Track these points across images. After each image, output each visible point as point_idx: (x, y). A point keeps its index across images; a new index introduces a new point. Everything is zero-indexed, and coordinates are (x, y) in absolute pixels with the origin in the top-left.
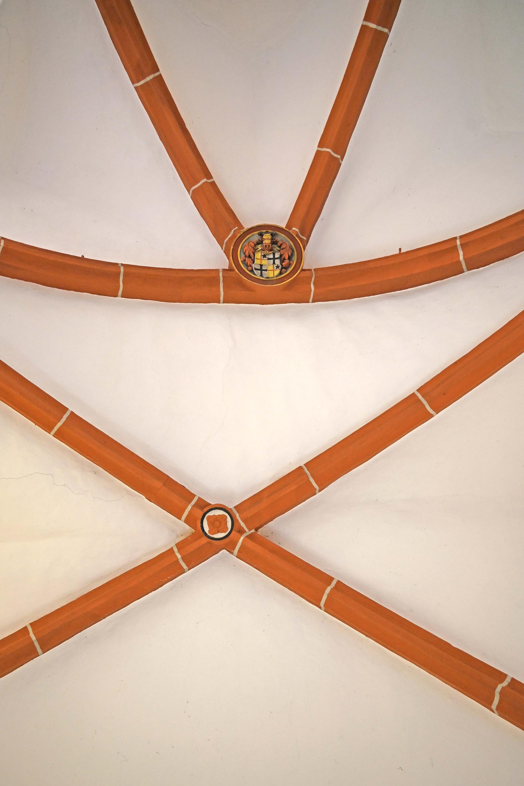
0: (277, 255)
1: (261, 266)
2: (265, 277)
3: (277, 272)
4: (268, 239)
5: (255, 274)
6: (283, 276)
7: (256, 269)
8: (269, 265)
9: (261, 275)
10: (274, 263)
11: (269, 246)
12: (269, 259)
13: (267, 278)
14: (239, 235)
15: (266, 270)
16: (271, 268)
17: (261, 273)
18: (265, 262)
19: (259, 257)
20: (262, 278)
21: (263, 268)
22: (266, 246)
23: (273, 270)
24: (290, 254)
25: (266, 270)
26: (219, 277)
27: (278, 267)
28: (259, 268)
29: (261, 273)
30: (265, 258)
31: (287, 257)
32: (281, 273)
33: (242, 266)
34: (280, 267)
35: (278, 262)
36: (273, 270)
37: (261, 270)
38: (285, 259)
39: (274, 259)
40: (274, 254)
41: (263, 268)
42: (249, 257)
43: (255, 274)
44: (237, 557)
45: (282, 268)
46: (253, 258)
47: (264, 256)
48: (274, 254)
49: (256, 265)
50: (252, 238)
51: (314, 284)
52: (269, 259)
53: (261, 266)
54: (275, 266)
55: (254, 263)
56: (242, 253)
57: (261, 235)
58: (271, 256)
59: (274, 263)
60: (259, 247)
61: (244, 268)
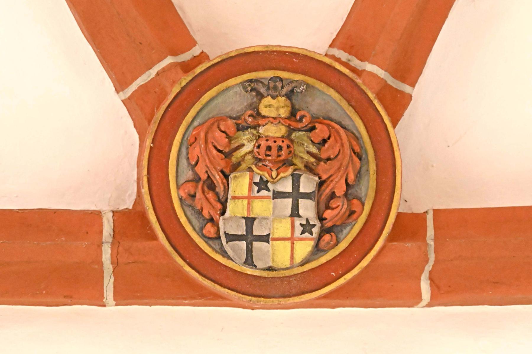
0: (307, 185)
1: (250, 221)
2: (260, 264)
3: (303, 248)
4: (276, 119)
5: (224, 254)
6: (323, 259)
7: (231, 238)
8: (278, 218)
9: (249, 261)
10: (295, 213)
11: (280, 148)
12: (277, 195)
13: (270, 269)
14: (176, 89)
15: (266, 239)
16: (282, 228)
17: (249, 250)
18: (262, 207)
19: (245, 192)
20: (249, 271)
21: (256, 232)
22: (269, 148)
23: (292, 240)
24: (352, 177)
25: (266, 239)
26: (101, 264)
27: (307, 228)
28: (242, 231)
29: (249, 250)
30: (264, 193)
31: (340, 191)
32: (317, 250)
33: (183, 220)
34: (315, 230)
35: (307, 209)
36: (292, 240)
37: (249, 237)
38: (333, 196)
39: (296, 195)
40: (296, 180)
41: (256, 232)
42: (212, 186)
43: (224, 254)
44: (116, 305)
45: (324, 231)
46: (220, 189)
47: (263, 185)
48: (296, 180)
49: (231, 223)
50: (220, 100)
51: (431, 279)
52: (277, 195)
53: (250, 221)
54: (298, 222)
55: (223, 213)
56: (184, 162)
57: (254, 89)
58: (287, 186)
59: (295, 213)
60: (247, 144)
61: (189, 229)
